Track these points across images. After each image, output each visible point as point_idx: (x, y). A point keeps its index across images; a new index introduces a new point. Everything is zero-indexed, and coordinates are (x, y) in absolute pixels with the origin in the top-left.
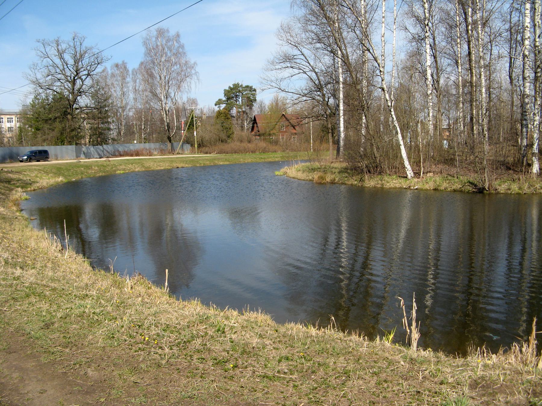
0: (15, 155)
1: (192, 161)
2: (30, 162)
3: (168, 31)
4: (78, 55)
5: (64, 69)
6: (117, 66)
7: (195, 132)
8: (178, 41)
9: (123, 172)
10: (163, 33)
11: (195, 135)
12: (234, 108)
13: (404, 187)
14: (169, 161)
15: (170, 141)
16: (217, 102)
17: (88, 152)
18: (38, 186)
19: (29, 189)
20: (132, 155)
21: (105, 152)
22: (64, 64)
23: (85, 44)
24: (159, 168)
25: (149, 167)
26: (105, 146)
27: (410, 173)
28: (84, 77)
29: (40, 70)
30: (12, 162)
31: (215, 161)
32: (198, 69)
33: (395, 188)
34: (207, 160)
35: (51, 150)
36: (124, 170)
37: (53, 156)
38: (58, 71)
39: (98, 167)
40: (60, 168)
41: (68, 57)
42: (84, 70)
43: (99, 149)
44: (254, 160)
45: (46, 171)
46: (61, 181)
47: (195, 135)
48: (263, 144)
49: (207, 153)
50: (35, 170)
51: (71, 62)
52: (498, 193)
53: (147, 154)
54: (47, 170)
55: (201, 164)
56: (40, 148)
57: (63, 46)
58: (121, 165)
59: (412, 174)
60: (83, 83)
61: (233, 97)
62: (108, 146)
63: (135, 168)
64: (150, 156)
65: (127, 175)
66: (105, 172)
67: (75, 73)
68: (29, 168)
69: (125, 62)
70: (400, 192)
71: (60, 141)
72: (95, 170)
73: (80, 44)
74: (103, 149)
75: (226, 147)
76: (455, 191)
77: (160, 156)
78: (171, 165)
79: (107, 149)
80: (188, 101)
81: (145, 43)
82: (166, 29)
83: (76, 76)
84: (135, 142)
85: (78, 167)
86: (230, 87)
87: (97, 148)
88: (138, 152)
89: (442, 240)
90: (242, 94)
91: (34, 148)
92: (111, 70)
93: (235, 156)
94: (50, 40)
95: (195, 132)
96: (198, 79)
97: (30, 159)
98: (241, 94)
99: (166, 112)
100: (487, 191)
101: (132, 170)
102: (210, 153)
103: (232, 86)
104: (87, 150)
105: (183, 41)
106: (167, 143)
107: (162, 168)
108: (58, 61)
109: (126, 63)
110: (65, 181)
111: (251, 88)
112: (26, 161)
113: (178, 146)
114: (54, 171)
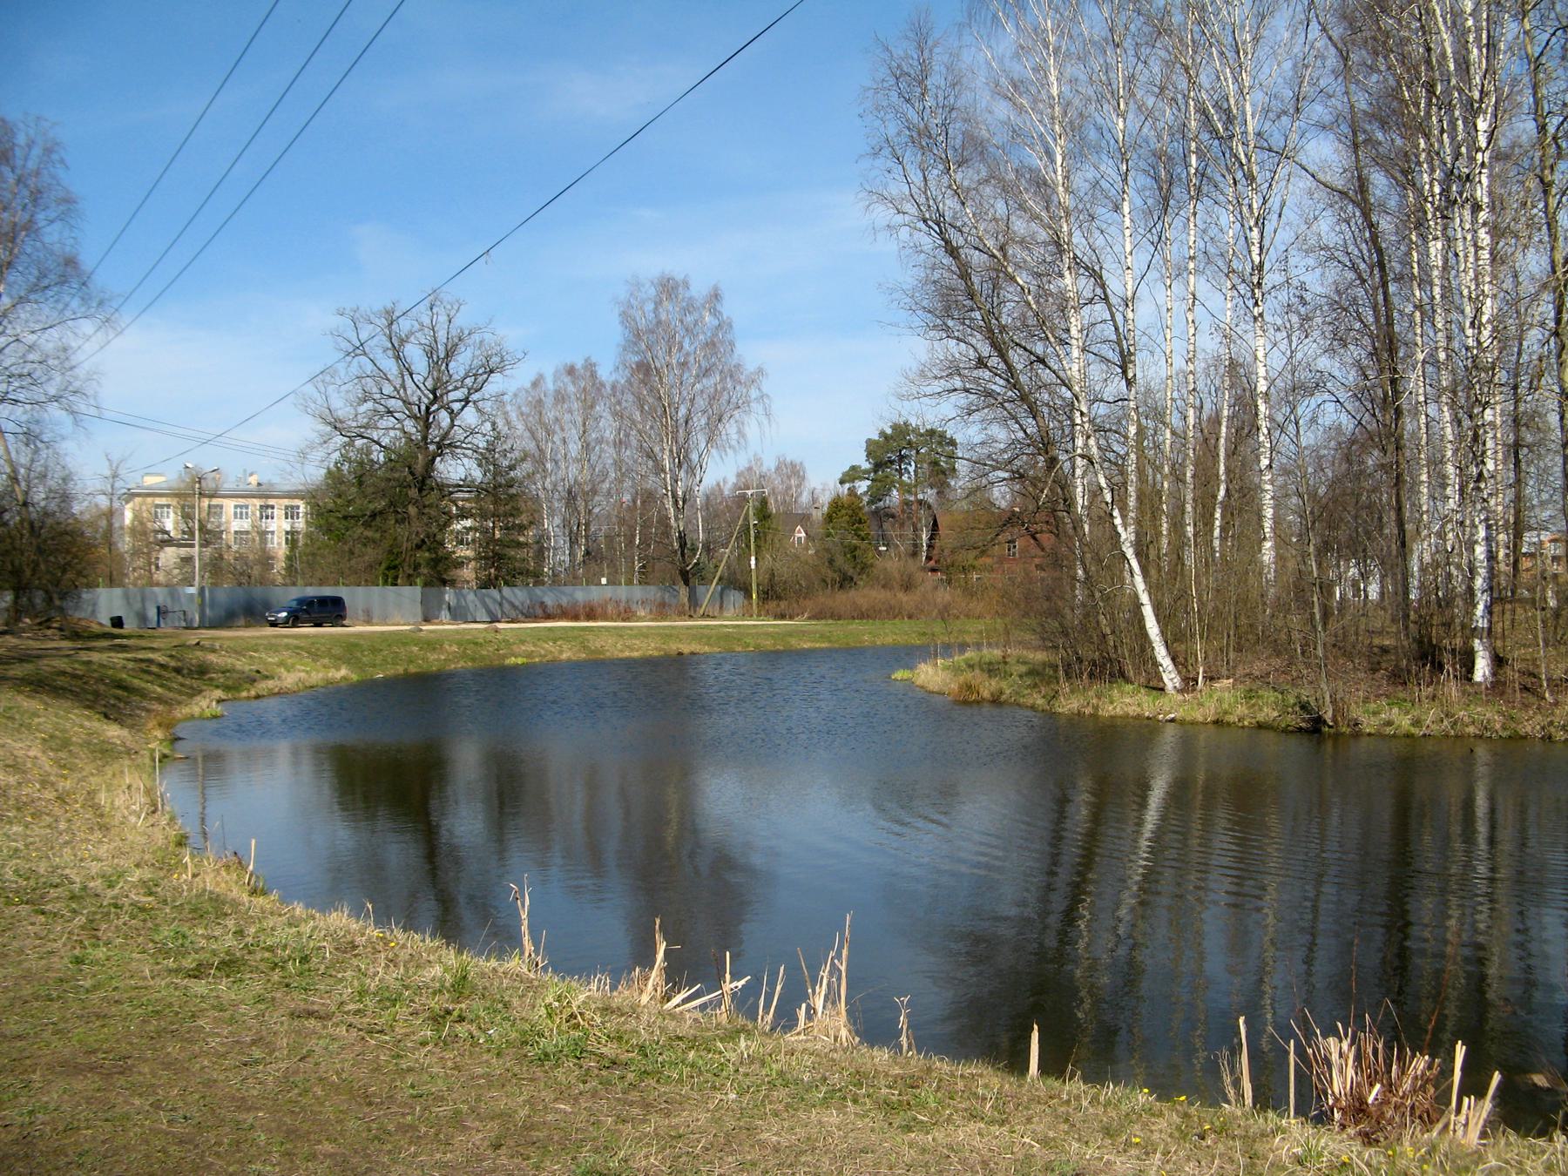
0: (260, 607)
1: (727, 636)
2: (294, 626)
3: (687, 285)
4: (441, 348)
5: (404, 386)
6: (571, 371)
7: (753, 558)
8: (715, 312)
9: (525, 660)
10: (675, 288)
11: (753, 567)
12: (895, 492)
13: (1147, 714)
14: (659, 635)
15: (686, 583)
16: (845, 474)
17: (459, 606)
18: (270, 686)
19: (244, 694)
20: (576, 618)
21: (506, 606)
22: (406, 373)
23: (459, 321)
24: (627, 654)
25: (601, 651)
26: (506, 591)
27: (1170, 677)
28: (456, 406)
29: (344, 388)
30: (247, 626)
31: (790, 639)
32: (766, 386)
33: (1127, 716)
34: (768, 634)
35: (354, 596)
36: (530, 655)
37: (360, 612)
38: (388, 389)
39: (459, 644)
40: (356, 645)
41: (415, 355)
42: (456, 388)
43: (489, 596)
44: (901, 639)
45: (313, 652)
46: (344, 678)
47: (753, 567)
48: (944, 595)
49: (783, 617)
50: (287, 647)
51: (420, 364)
52: (1357, 735)
53: (619, 615)
54: (318, 649)
55: (748, 646)
56: (328, 591)
57: (404, 326)
58: (523, 642)
59: (1177, 681)
60: (452, 421)
61: (892, 462)
62: (516, 590)
63: (561, 652)
64: (624, 620)
65: (549, 670)
66: (473, 660)
67: (431, 396)
68: (273, 641)
69: (594, 360)
70: (1148, 729)
71: (392, 572)
72: (449, 654)
73: (446, 318)
74: (502, 597)
75: (842, 599)
76: (1260, 726)
77: (652, 620)
78: (665, 647)
79: (513, 600)
80: (778, 468)
81: (626, 317)
82: (679, 277)
83: (432, 403)
84: (604, 581)
85: (405, 644)
86: (882, 433)
87: (484, 595)
88: (592, 609)
89: (1022, 826)
90: (918, 452)
91: (312, 592)
92: (555, 382)
93: (856, 626)
94: (375, 309)
95: (753, 558)
96: (768, 415)
97: (295, 619)
98: (914, 452)
99: (676, 502)
100: (1330, 727)
101: (549, 657)
102: (791, 618)
103: (889, 431)
104: (458, 600)
105: (728, 309)
106: (676, 587)
107: (636, 654)
108: (390, 366)
109: (595, 365)
110: (355, 677)
111: (942, 435)
112: (284, 623)
113: (708, 592)
114: (337, 651)
